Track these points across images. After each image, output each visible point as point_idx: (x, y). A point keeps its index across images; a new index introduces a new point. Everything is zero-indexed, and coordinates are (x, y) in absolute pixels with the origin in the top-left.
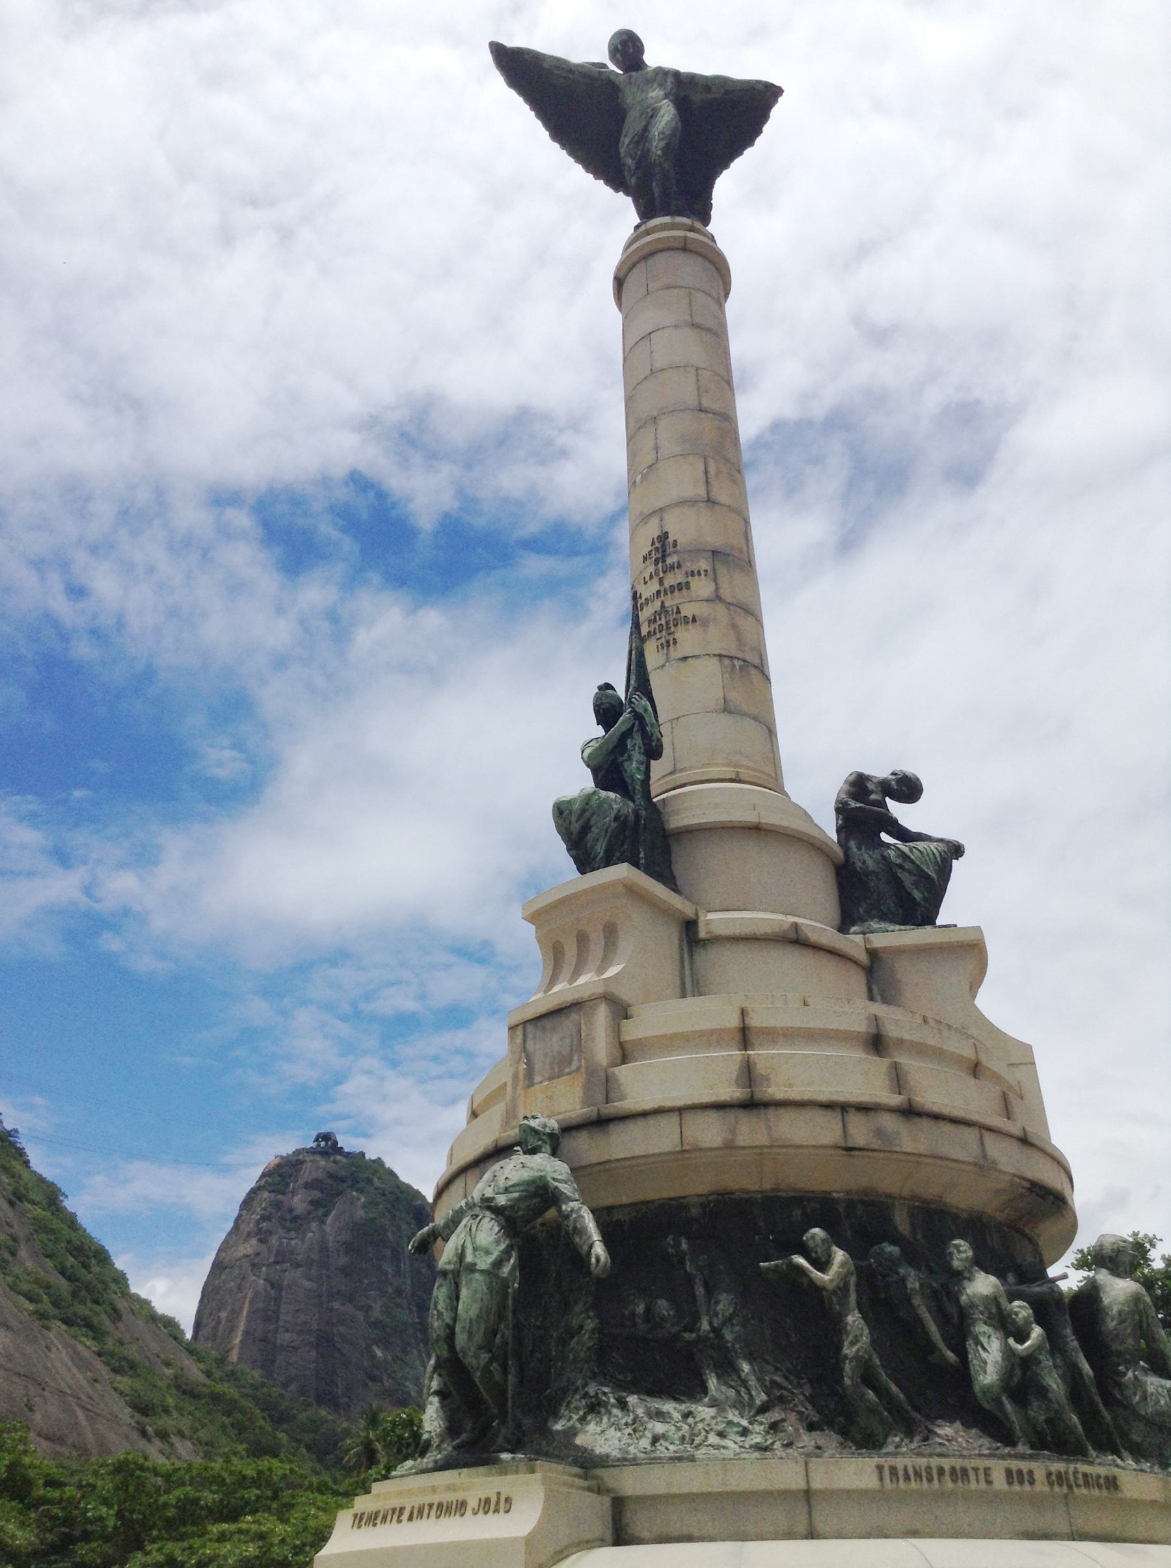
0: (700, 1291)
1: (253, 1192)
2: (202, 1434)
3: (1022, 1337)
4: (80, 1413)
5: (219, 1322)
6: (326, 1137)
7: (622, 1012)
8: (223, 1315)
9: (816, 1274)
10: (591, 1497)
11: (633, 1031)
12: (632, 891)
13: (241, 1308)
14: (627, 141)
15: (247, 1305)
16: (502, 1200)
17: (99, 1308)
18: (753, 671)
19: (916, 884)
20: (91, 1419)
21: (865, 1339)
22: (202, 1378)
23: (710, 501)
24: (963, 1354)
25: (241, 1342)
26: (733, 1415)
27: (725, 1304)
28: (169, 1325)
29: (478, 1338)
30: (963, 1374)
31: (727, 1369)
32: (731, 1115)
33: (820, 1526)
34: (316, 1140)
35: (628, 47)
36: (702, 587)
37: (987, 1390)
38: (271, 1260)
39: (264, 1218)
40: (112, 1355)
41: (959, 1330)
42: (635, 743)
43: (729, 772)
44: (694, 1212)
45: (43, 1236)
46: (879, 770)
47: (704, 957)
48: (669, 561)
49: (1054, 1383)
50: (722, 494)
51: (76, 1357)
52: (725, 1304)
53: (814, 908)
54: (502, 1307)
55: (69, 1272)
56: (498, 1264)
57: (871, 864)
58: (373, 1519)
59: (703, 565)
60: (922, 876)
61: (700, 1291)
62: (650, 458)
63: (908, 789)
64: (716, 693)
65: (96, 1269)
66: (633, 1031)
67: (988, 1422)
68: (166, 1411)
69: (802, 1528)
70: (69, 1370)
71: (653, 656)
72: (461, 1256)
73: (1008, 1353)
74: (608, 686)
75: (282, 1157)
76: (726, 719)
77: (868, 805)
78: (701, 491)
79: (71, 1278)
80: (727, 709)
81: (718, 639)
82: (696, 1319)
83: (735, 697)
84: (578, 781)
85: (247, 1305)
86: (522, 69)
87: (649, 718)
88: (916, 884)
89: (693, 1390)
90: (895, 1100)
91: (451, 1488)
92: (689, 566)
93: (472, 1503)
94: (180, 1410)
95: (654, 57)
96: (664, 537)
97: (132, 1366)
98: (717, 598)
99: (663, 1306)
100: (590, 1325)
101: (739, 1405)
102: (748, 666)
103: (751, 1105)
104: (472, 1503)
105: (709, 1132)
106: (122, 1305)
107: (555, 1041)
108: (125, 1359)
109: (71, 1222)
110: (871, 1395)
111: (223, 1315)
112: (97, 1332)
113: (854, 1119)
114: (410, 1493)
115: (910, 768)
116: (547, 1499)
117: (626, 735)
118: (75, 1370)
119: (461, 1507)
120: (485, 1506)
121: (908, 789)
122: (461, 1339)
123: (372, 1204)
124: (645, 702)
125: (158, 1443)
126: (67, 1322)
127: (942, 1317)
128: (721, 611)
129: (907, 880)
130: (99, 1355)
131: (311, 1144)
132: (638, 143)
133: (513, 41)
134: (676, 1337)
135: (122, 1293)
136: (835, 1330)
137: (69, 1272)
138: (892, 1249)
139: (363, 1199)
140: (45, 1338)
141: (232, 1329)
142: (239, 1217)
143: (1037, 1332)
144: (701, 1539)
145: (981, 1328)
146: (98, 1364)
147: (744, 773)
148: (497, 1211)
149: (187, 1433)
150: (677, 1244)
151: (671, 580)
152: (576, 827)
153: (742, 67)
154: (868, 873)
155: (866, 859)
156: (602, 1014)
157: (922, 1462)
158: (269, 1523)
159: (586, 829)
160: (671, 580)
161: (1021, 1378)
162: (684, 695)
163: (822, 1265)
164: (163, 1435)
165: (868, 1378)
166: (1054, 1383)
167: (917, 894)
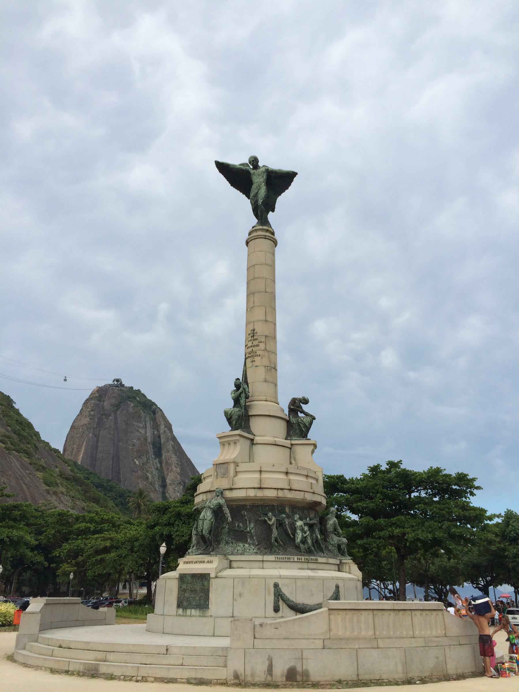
0: (248, 522)
1: (87, 401)
2: (71, 493)
3: (305, 533)
4: (24, 486)
5: (73, 449)
6: (118, 380)
7: (237, 465)
8: (75, 446)
9: (269, 522)
10: (226, 561)
11: (239, 469)
12: (240, 435)
13: (83, 444)
14: (252, 195)
15: (85, 443)
16: (212, 507)
17: (29, 446)
18: (273, 369)
19: (304, 427)
20: (28, 488)
21: (276, 534)
22: (70, 473)
23: (266, 321)
24: (294, 536)
25: (82, 457)
26: (252, 546)
27: (252, 525)
28: (56, 451)
29: (207, 532)
30: (294, 540)
31: (252, 537)
32: (256, 490)
33: (264, 567)
34: (114, 381)
35: (254, 161)
36: (262, 346)
37: (297, 543)
38: (95, 426)
39: (92, 410)
40: (35, 464)
41: (294, 530)
42: (243, 395)
43: (264, 398)
44: (248, 507)
45: (6, 418)
46: (300, 396)
47: (255, 448)
48: (255, 337)
49: (309, 541)
50: (269, 319)
51: (22, 465)
52: (252, 525)
53: (281, 427)
54: (211, 527)
55: (17, 432)
56: (211, 519)
57: (294, 422)
58: (187, 563)
59: (263, 339)
60: (305, 426)
61: (248, 522)
62: (252, 305)
63: (306, 401)
64: (262, 377)
65: (27, 431)
66: (239, 469)
67: (297, 548)
68: (57, 484)
69: (261, 566)
70: (20, 470)
71: (249, 364)
72: (204, 517)
73: (303, 536)
74: (238, 379)
75: (99, 387)
76: (265, 384)
77: (296, 406)
78: (264, 318)
79: (19, 435)
80: (266, 381)
81: (265, 362)
82: (247, 527)
83: (268, 378)
84: (230, 404)
85: (85, 443)
86: (224, 168)
87: (247, 390)
88: (304, 427)
89: (246, 542)
90: (288, 487)
91: (202, 558)
92: (259, 340)
93: (206, 561)
94: (62, 484)
95: (260, 164)
96: (254, 330)
97: (43, 467)
98: (266, 349)
99: (241, 524)
100: (227, 527)
101: (253, 544)
102: (272, 368)
103: (260, 488)
104: (206, 561)
105: (252, 493)
106: (38, 445)
107: (221, 470)
108: (40, 466)
109: (17, 412)
110: (276, 544)
111: (75, 446)
112: (29, 455)
113: (279, 491)
114: (194, 558)
115: (306, 397)
116: (219, 562)
117: (241, 393)
118: (21, 470)
119: (204, 562)
120: (208, 562)
121: (306, 401)
122: (204, 532)
123: (136, 406)
124: (246, 386)
125: (54, 497)
126: (17, 451)
127: (292, 529)
128: (266, 353)
129: (302, 426)
130: (31, 464)
131: (111, 382)
132: (255, 197)
133: (221, 160)
134: (243, 531)
135: (38, 440)
136: (271, 531)
137: (17, 432)
138: (284, 516)
139: (132, 405)
140: (9, 458)
141: (79, 451)
142: (82, 409)
143: (308, 533)
144: (245, 568)
145: (298, 531)
146: (31, 467)
147: (268, 399)
148: (211, 508)
149: (65, 493)
150: (244, 513)
151: (256, 343)
152: (229, 417)
153: (286, 167)
154: (294, 424)
155: (293, 420)
156: (232, 467)
157: (283, 556)
158: (113, 535)
159: (231, 417)
160: (256, 343)
161: (304, 541)
162: (256, 377)
163: (270, 520)
164: (55, 493)
165: (276, 540)
166: (309, 541)
167: (304, 429)
